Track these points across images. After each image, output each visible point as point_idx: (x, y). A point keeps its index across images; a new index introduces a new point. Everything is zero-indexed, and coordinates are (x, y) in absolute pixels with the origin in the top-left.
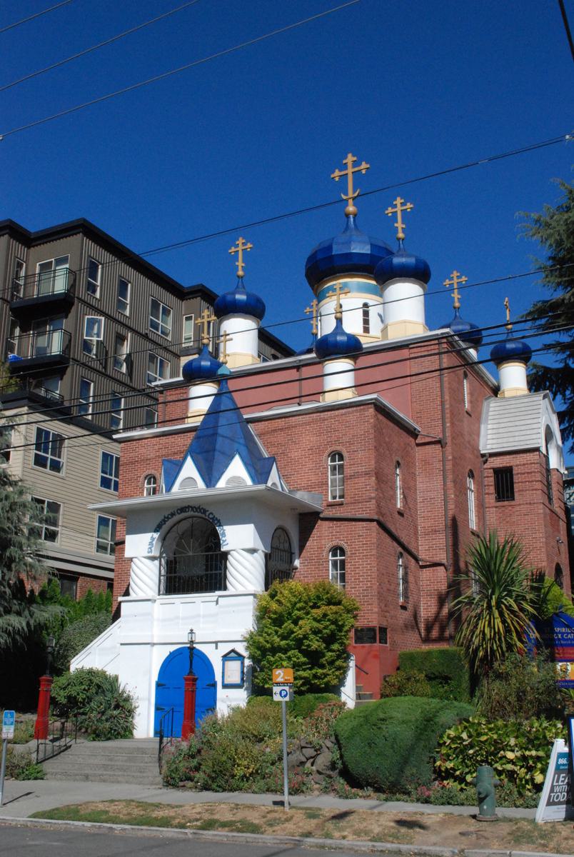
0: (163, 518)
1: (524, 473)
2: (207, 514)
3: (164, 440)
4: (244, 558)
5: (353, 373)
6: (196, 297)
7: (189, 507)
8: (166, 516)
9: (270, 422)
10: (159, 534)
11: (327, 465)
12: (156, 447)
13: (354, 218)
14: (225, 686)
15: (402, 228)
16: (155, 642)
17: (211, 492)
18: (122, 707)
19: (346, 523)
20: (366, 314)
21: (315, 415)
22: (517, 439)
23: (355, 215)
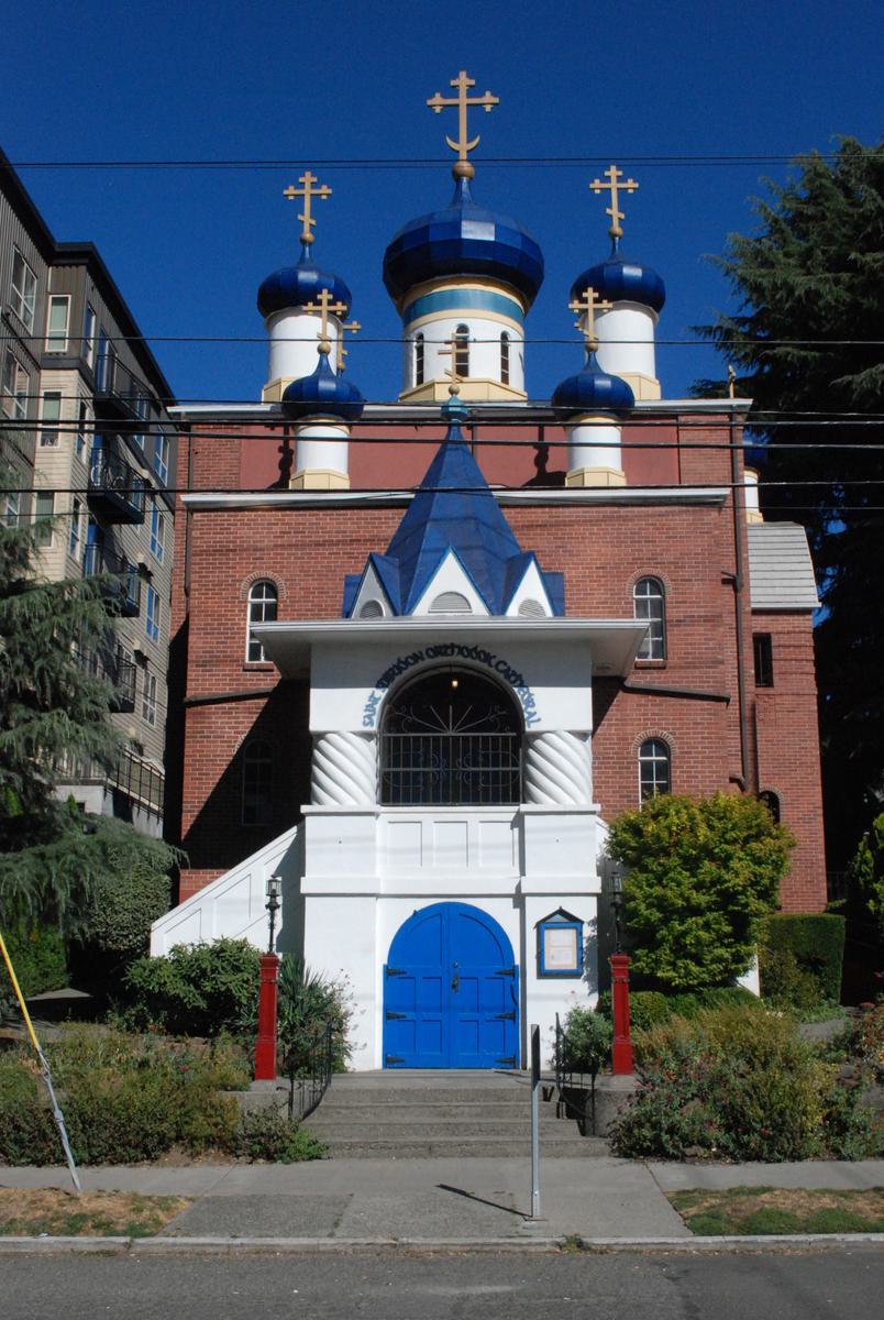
0: (395, 662)
1: (789, 646)
2: (494, 662)
3: (292, 516)
4: (571, 746)
5: (346, 444)
6: (77, 265)
7: (453, 646)
8: (403, 659)
9: (519, 510)
10: (387, 690)
11: (246, 602)
12: (276, 529)
13: (469, 182)
14: (543, 974)
15: (311, 225)
16: (382, 892)
17: (497, 623)
18: (324, 1013)
19: (673, 700)
20: (505, 351)
21: (608, 509)
22: (778, 591)
23: (471, 179)
